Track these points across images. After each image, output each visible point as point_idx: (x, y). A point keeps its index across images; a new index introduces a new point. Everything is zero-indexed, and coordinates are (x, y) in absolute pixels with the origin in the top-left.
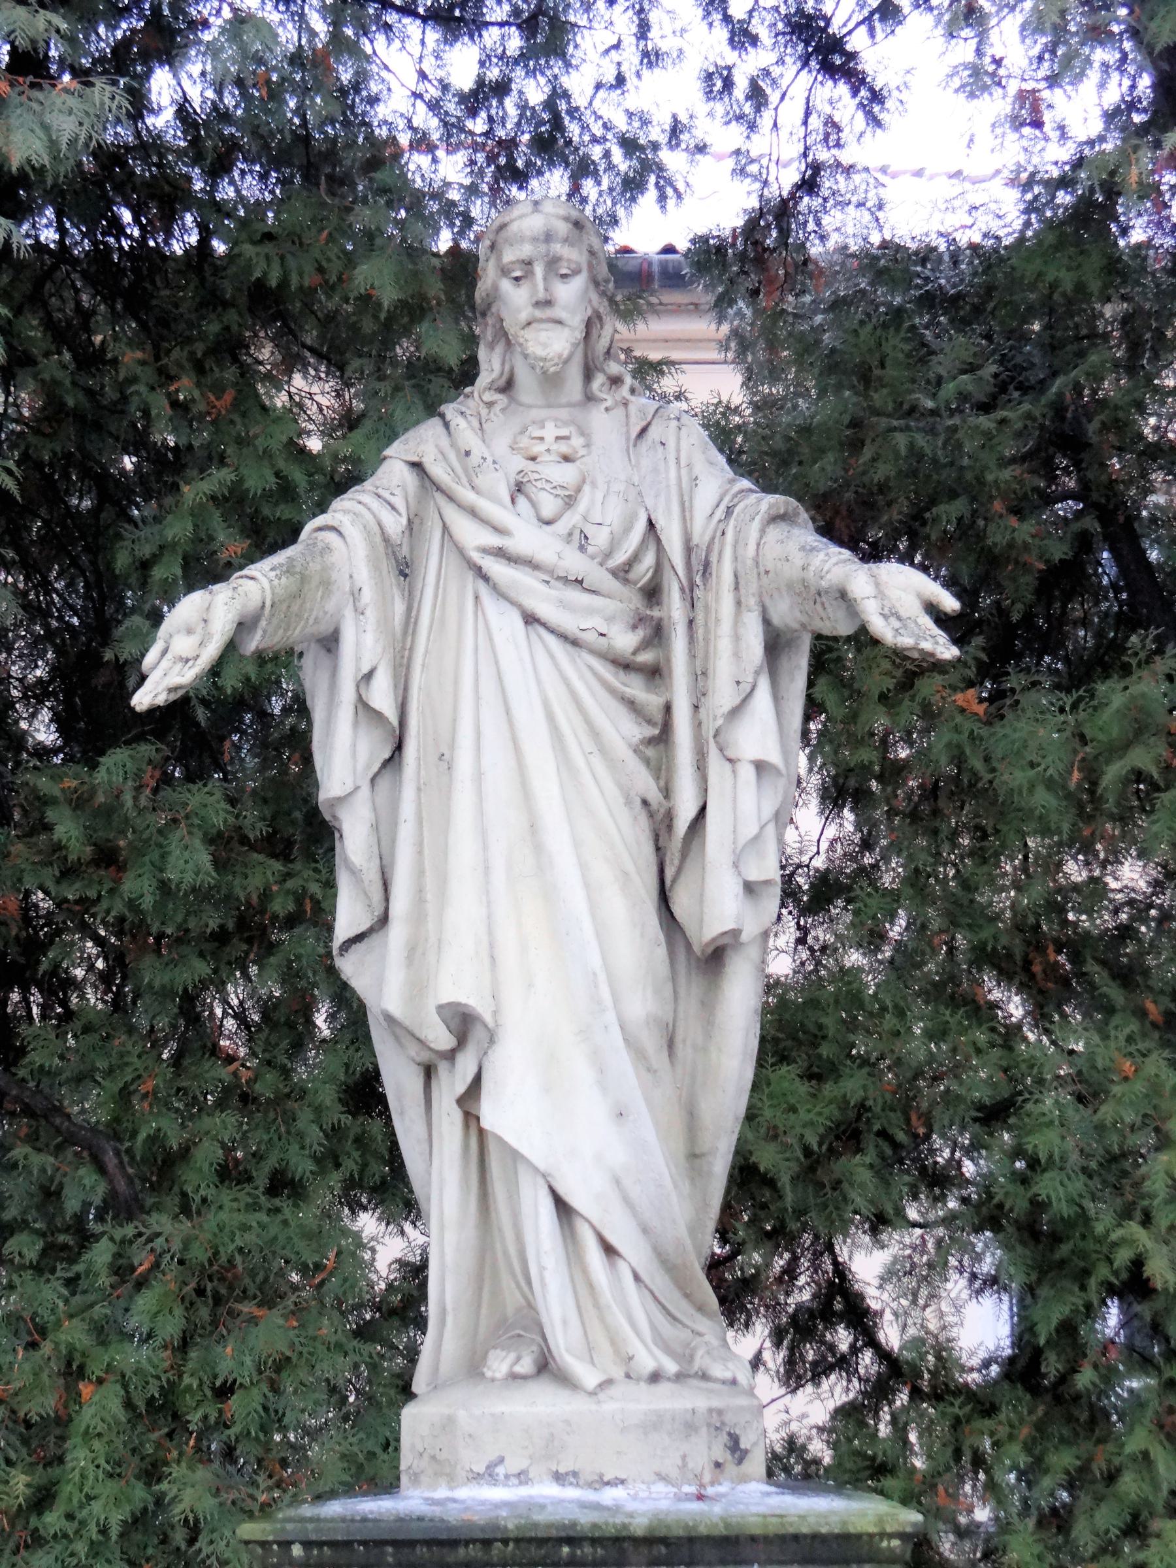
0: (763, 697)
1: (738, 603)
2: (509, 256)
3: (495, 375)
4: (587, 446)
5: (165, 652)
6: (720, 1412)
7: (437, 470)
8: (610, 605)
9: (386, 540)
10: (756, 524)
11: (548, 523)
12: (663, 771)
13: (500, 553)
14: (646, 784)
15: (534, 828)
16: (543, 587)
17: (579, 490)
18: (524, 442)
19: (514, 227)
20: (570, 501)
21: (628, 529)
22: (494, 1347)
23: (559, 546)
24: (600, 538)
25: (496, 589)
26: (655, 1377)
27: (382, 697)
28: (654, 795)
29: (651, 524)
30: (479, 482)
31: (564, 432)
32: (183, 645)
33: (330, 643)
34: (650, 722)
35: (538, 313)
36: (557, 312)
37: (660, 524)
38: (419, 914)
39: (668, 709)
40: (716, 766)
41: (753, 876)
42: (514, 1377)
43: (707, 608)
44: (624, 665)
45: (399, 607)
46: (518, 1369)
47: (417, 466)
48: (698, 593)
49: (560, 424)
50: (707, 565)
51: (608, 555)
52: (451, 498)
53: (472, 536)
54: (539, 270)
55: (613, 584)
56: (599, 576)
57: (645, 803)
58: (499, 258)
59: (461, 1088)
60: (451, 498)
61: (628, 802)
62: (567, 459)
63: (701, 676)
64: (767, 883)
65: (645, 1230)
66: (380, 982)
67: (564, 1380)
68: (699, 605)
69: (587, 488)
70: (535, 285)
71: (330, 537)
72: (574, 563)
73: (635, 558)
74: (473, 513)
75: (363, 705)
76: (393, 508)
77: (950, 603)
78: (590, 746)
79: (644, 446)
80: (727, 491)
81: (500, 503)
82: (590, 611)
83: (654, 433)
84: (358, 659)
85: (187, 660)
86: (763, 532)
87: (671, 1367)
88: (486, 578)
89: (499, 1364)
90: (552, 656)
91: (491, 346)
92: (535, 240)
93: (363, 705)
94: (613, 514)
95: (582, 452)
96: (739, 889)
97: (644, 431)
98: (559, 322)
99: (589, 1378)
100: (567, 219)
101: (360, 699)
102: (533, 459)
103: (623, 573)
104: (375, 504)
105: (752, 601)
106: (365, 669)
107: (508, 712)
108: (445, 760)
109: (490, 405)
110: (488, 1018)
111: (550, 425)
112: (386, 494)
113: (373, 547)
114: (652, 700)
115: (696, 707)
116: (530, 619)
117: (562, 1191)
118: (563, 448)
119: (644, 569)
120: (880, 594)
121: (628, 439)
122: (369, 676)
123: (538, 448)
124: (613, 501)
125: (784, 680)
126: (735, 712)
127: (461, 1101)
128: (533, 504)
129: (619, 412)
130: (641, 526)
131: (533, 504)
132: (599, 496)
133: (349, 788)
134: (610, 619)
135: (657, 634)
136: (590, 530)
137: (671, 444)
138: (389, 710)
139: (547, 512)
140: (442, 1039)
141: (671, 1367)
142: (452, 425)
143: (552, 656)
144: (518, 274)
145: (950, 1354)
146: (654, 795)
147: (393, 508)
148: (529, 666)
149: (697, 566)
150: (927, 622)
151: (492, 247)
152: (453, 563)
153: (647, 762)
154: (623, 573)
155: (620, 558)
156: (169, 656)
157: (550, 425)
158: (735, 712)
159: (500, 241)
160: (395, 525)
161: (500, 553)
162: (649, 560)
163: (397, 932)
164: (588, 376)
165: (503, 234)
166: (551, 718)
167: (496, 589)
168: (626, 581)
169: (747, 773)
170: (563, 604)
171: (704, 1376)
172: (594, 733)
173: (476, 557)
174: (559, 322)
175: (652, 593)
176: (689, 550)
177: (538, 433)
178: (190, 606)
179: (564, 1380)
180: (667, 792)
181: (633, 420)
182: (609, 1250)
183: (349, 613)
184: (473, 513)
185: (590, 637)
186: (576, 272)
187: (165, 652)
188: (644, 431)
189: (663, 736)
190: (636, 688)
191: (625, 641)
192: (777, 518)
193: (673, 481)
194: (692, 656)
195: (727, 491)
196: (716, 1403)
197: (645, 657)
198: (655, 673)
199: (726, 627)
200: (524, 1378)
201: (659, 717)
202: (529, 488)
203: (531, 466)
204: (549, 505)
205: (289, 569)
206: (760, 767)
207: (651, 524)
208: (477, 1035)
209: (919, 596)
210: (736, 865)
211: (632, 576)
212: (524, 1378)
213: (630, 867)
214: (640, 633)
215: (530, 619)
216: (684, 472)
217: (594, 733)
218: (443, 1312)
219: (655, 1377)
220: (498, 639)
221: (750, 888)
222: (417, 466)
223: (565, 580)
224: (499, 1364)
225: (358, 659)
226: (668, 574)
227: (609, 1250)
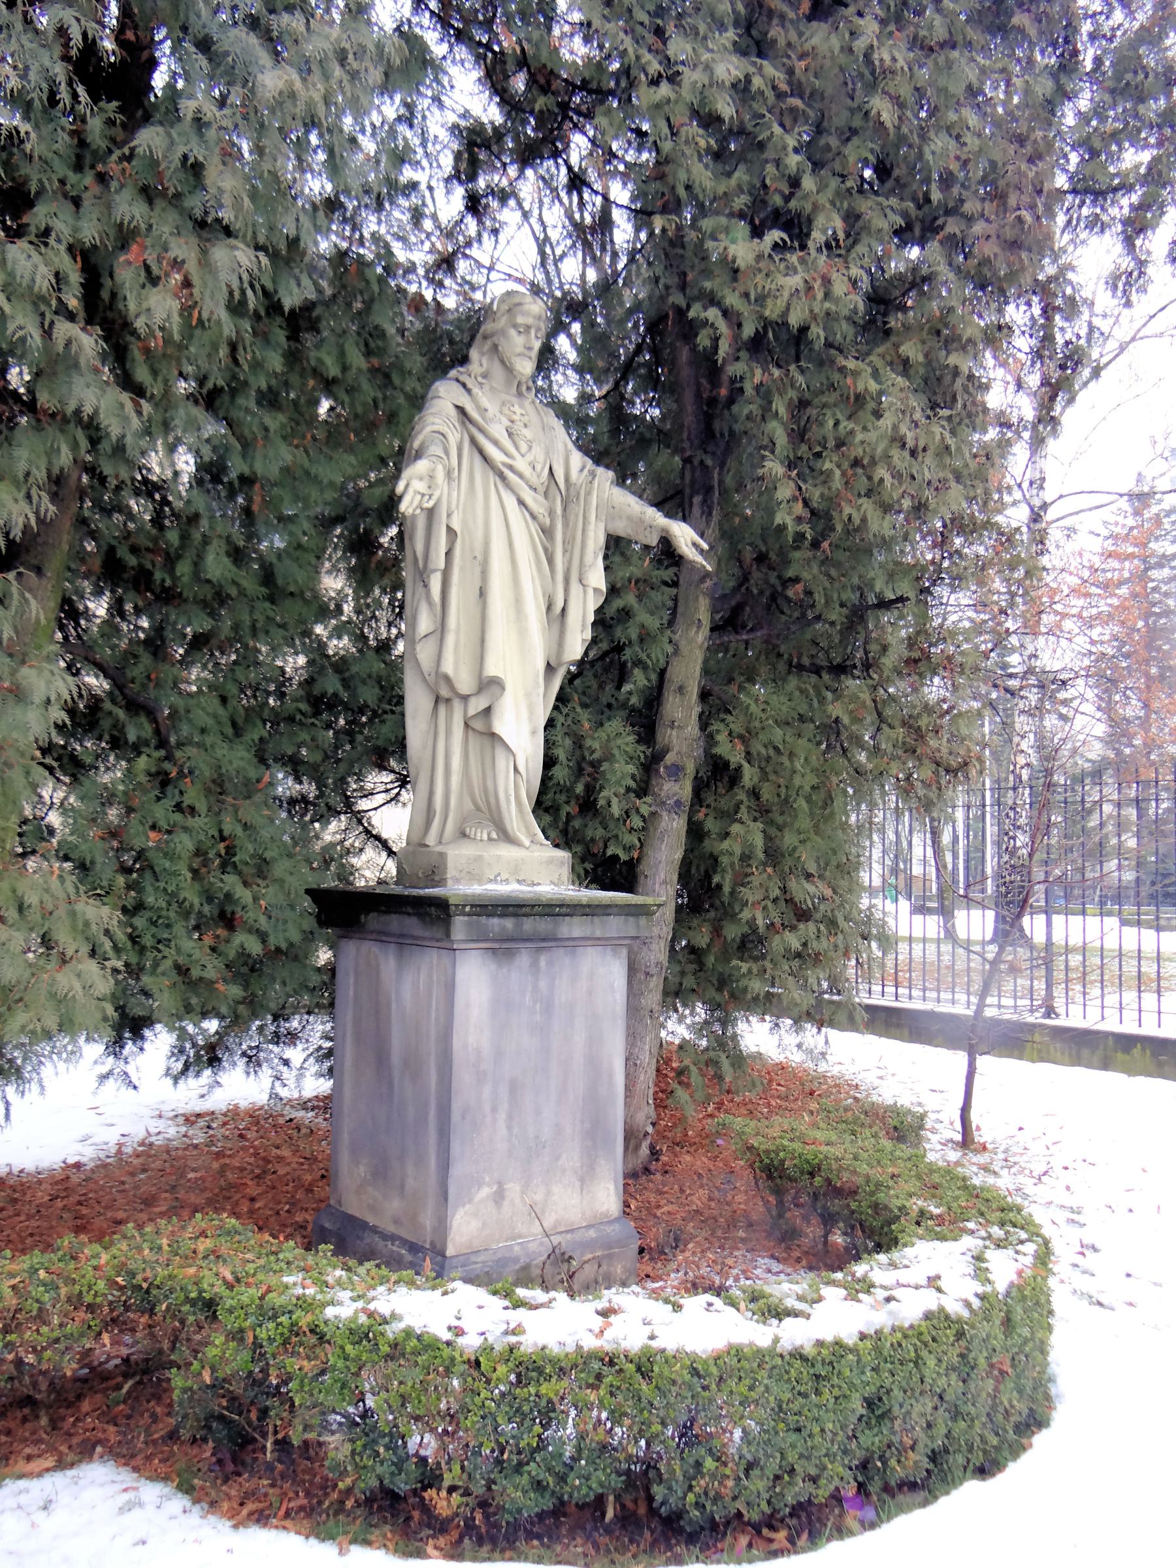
37: (555, 468)
40: (575, 587)
149: (572, 492)
161: (511, 468)
206: (596, 590)
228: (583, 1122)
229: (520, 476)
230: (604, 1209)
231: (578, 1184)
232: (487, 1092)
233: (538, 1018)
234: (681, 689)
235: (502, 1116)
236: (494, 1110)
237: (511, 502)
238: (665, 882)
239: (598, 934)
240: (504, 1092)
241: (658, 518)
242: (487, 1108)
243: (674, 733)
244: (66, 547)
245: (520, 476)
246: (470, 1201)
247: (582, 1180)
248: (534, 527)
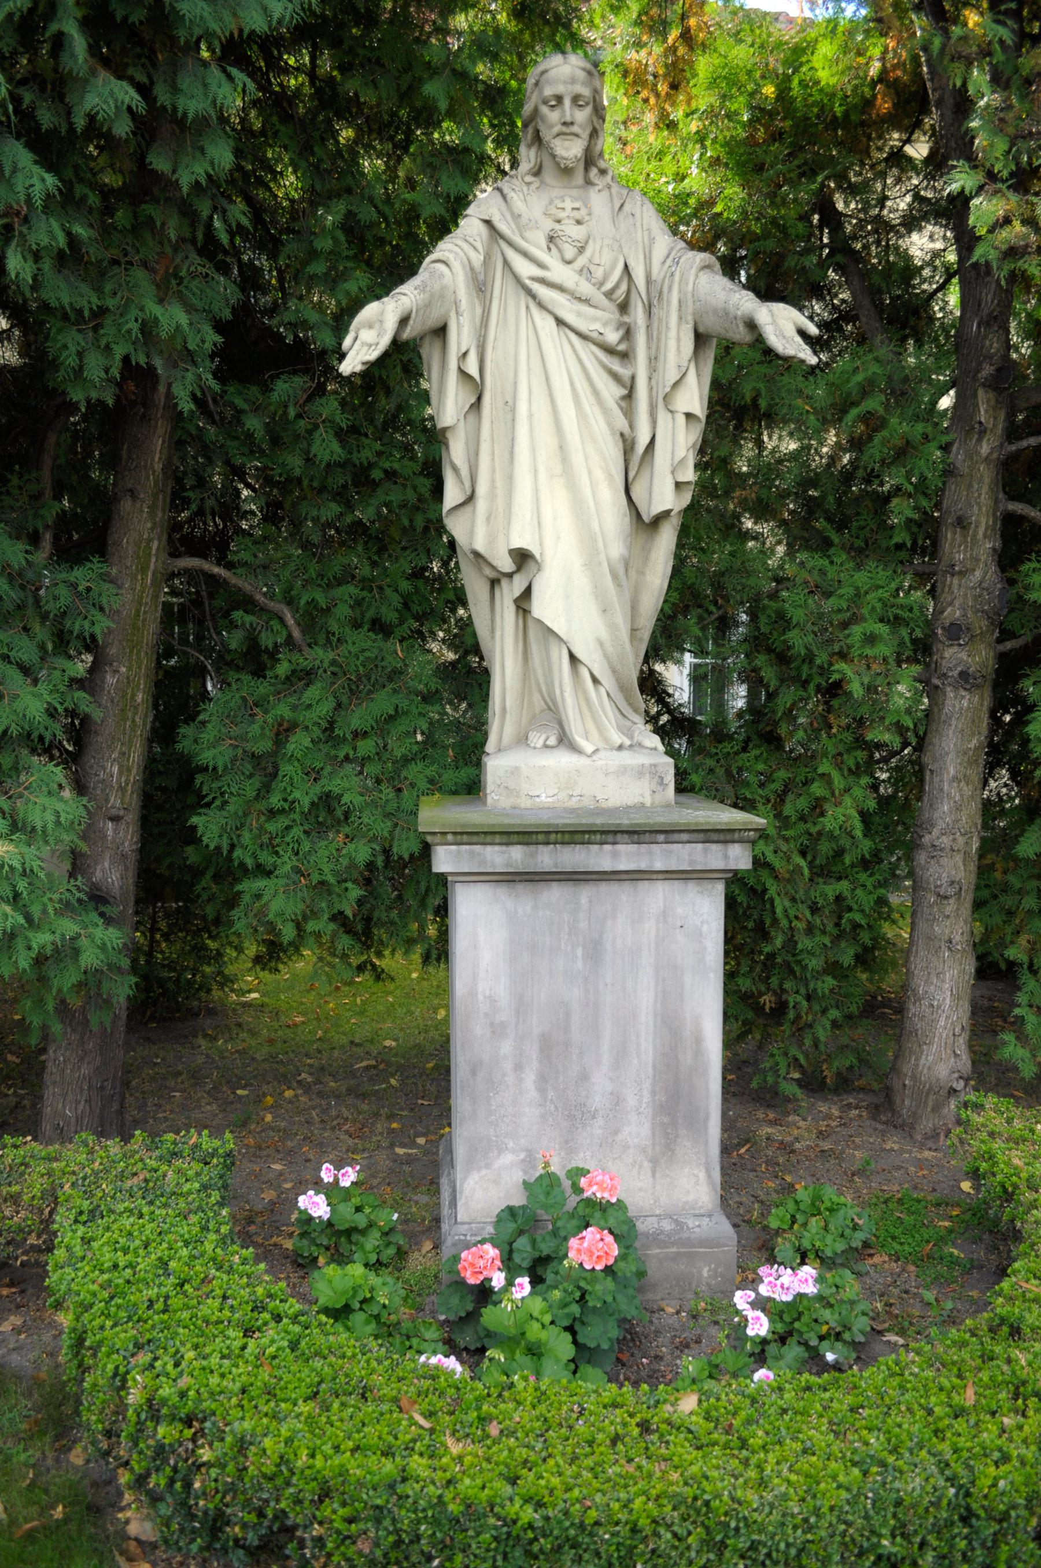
0: (692, 377)
1: (680, 318)
2: (548, 92)
3: (532, 165)
4: (590, 214)
5: (356, 339)
6: (655, 766)
7: (502, 226)
8: (606, 315)
9: (472, 269)
10: (693, 271)
11: (569, 263)
12: (629, 412)
13: (542, 281)
14: (621, 423)
15: (562, 448)
16: (568, 303)
17: (587, 242)
18: (554, 211)
19: (553, 73)
20: (581, 250)
21: (613, 267)
22: (532, 730)
23: (576, 277)
24: (599, 273)
25: (541, 306)
26: (620, 747)
27: (473, 369)
28: (626, 430)
29: (626, 266)
30: (527, 234)
31: (577, 205)
32: (367, 335)
33: (441, 332)
34: (624, 386)
35: (564, 129)
36: (575, 129)
37: (632, 264)
38: (492, 495)
39: (633, 378)
40: (662, 416)
41: (681, 479)
42: (546, 746)
43: (660, 320)
44: (610, 351)
45: (479, 311)
46: (549, 743)
47: (488, 223)
48: (654, 310)
49: (575, 199)
50: (661, 293)
51: (601, 284)
52: (510, 244)
53: (525, 269)
54: (567, 102)
55: (605, 302)
56: (599, 298)
57: (622, 435)
58: (541, 91)
59: (517, 593)
60: (510, 244)
61: (613, 434)
62: (579, 222)
63: (653, 362)
64: (688, 483)
65: (614, 671)
66: (472, 533)
67: (574, 748)
68: (655, 318)
69: (591, 242)
70: (564, 111)
71: (441, 267)
72: (586, 288)
73: (617, 286)
74: (525, 254)
75: (463, 374)
76: (475, 248)
77: (813, 330)
78: (592, 400)
79: (622, 215)
80: (672, 249)
81: (539, 248)
82: (595, 319)
83: (627, 208)
84: (459, 344)
85: (370, 346)
86: (697, 276)
87: (628, 742)
88: (534, 296)
89: (537, 739)
90: (575, 351)
91: (529, 146)
92: (565, 82)
93: (463, 374)
94: (606, 258)
95: (587, 218)
96: (673, 486)
97: (622, 205)
98: (577, 135)
99: (589, 748)
100: (584, 69)
101: (459, 368)
102: (559, 221)
103: (609, 294)
104: (465, 246)
105: (690, 318)
106: (463, 350)
107: (547, 379)
108: (511, 408)
109: (528, 184)
110: (538, 556)
111: (568, 200)
112: (471, 240)
113: (466, 274)
114: (625, 372)
115: (650, 379)
116: (560, 322)
117: (575, 651)
118: (577, 215)
119: (620, 294)
120: (774, 323)
121: (613, 211)
122: (465, 354)
123: (562, 215)
124: (605, 250)
125: (702, 364)
126: (676, 384)
127: (516, 601)
128: (560, 250)
129: (605, 193)
130: (620, 266)
131: (560, 250)
132: (598, 249)
133: (455, 421)
134: (605, 324)
135: (628, 334)
136: (593, 268)
137: (638, 215)
138: (921, 733)
139: (569, 256)
140: (506, 564)
141: (628, 742)
142: (509, 197)
143: (575, 351)
144: (553, 103)
145: (434, 426)
146: (626, 430)
147: (475, 248)
148: (670, 433)
149: (654, 294)
150: (798, 339)
151: (537, 84)
152: (511, 285)
153: (621, 409)
154: (609, 294)
155: (609, 285)
156: (358, 342)
157: (568, 200)
158: (676, 384)
159: (542, 80)
160: (477, 259)
161: (542, 281)
162: (624, 287)
163: (481, 504)
164: (587, 169)
165: (545, 76)
166: (572, 384)
167: (541, 306)
168: (611, 300)
169: (681, 419)
170: (579, 314)
171: (640, 745)
172: (596, 392)
173: (528, 282)
174: (577, 135)
175: (624, 307)
176: (649, 281)
177: (560, 205)
178: (370, 310)
179: (574, 748)
180: (631, 426)
181: (616, 199)
182: (595, 680)
183: (453, 315)
184: (525, 254)
185: (595, 335)
186: (587, 104)
187: (356, 339)
188: (622, 205)
189: (629, 396)
190: (616, 365)
191: (612, 337)
192: (707, 267)
193: (640, 240)
194: (649, 348)
195: (672, 249)
196: (653, 761)
197: (622, 347)
198: (625, 356)
199: (673, 333)
200: (552, 747)
201: (628, 384)
202: (558, 241)
203: (557, 227)
204: (570, 252)
205: (422, 288)
206: (689, 416)
207: (626, 266)
208: (531, 566)
209: (795, 324)
210: (673, 473)
211: (614, 296)
212: (552, 747)
213: (614, 472)
214: (621, 332)
215: (560, 322)
216: (646, 233)
217: (596, 392)
218: (504, 710)
219: (620, 747)
220: (543, 338)
221: (678, 485)
222: (488, 223)
223: (580, 299)
224: (537, 739)
225: (459, 344)
226: (634, 296)
227: (595, 680)
228: (653, 1093)
229: (560, 288)
230: (691, 1197)
231: (647, 1165)
232: (506, 1047)
233: (580, 964)
234: (961, 523)
235: (530, 1078)
236: (518, 1067)
237: (546, 324)
238: (955, 779)
239: (659, 866)
240: (533, 1051)
241: (746, 302)
242: (508, 1066)
243: (956, 581)
244: (158, 467)
245: (560, 288)
246: (488, 1166)
247: (655, 1162)
248: (588, 353)
